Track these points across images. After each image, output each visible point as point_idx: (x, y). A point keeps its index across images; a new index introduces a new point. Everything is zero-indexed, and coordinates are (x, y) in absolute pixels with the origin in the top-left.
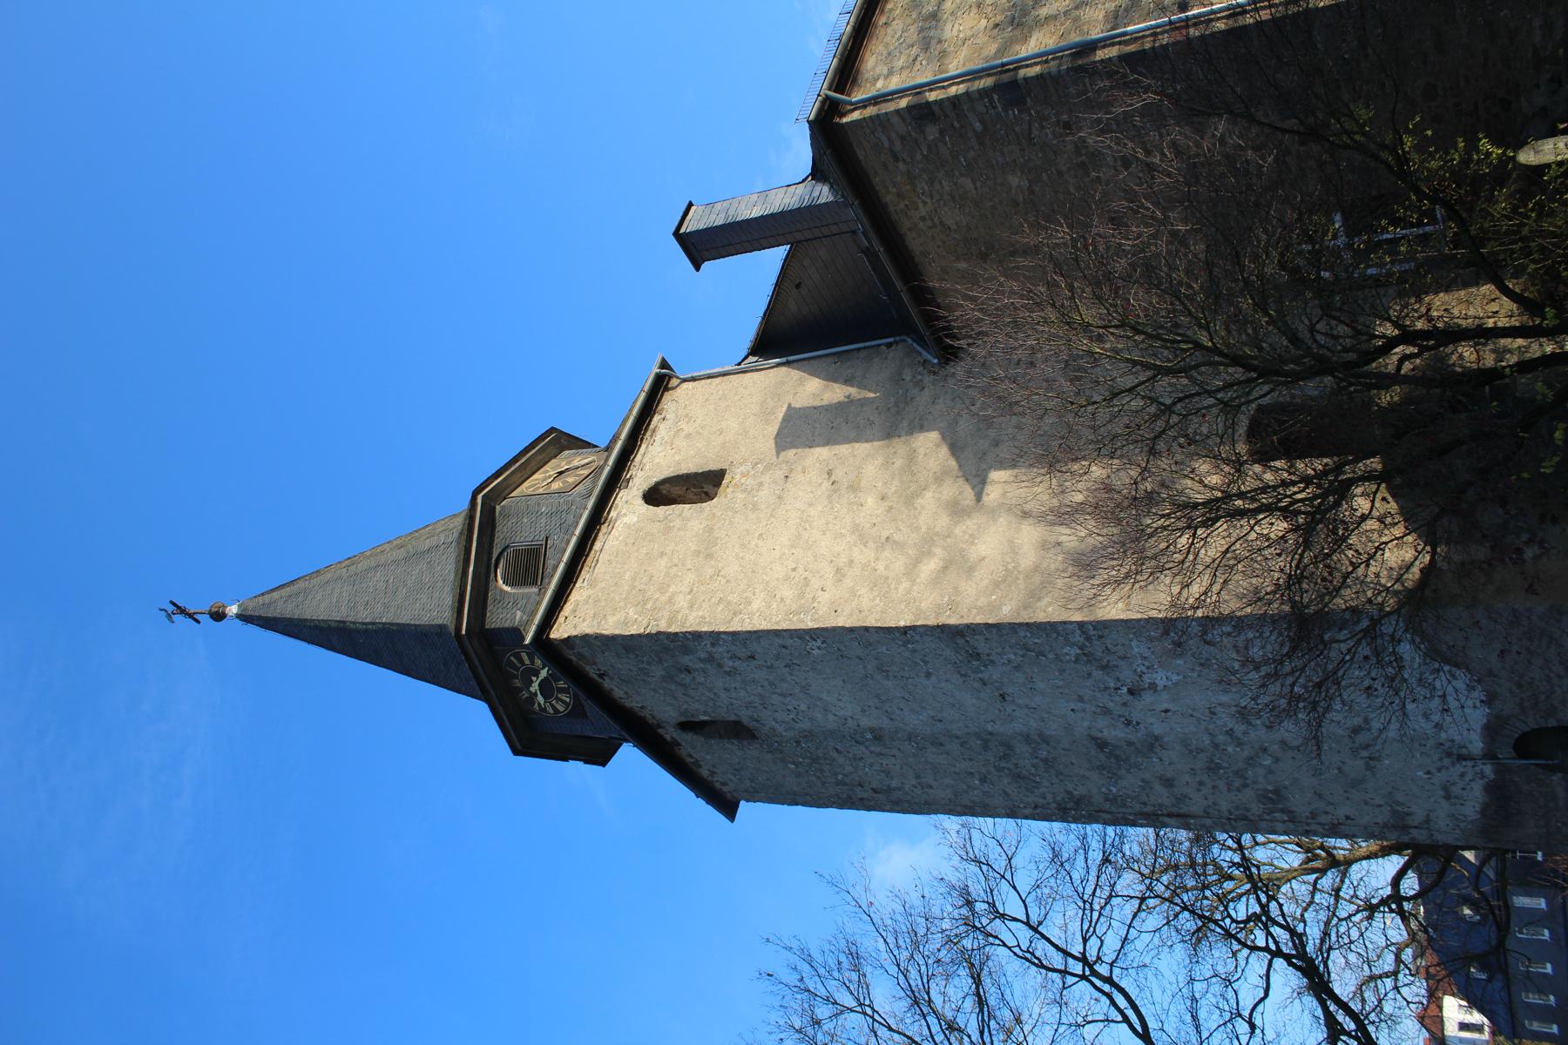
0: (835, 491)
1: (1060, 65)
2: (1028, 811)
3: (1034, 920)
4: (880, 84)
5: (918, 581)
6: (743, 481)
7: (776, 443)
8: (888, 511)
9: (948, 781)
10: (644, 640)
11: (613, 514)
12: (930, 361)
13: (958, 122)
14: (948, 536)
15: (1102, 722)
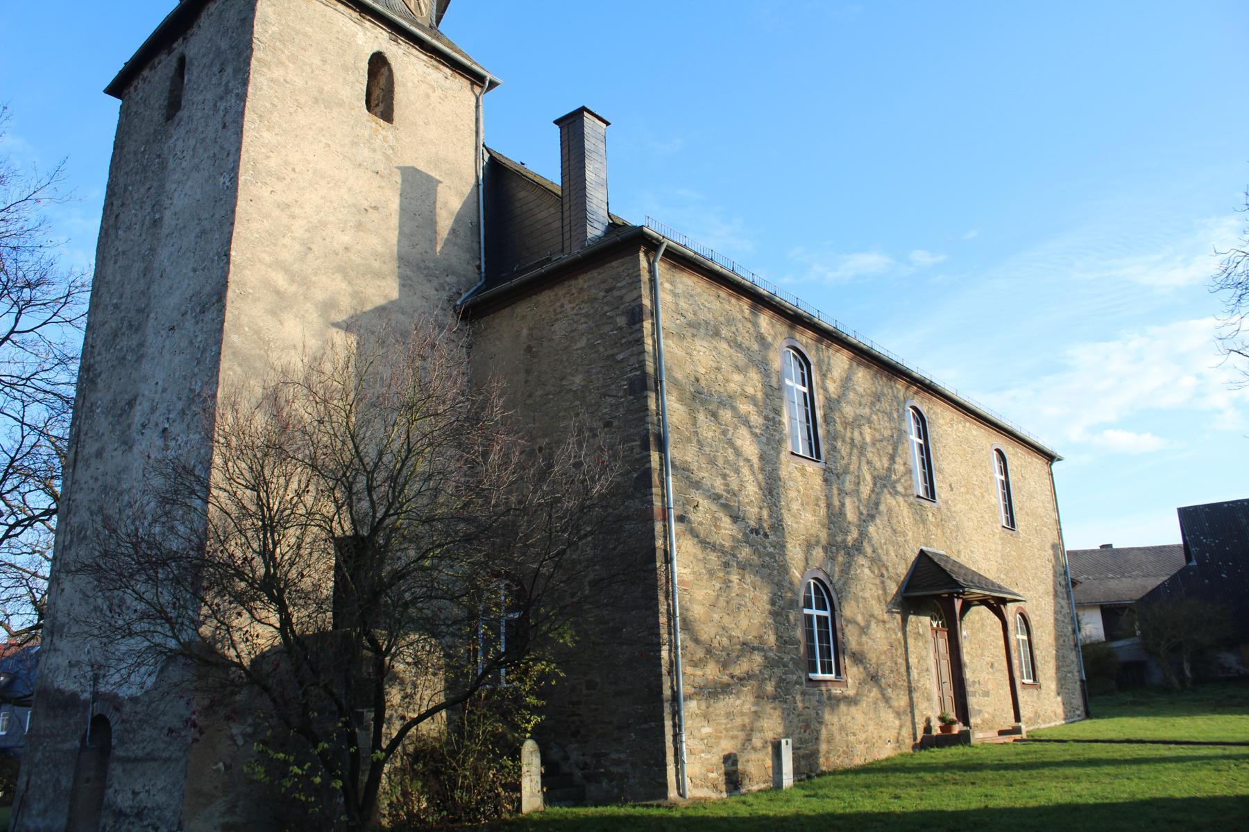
0: (359, 211)
1: (652, 424)
2: (90, 340)
3: (15, 337)
4: (667, 286)
5: (270, 270)
6: (380, 136)
7: (409, 168)
8: (334, 251)
9: (118, 278)
10: (249, 37)
11: (368, 24)
12: (459, 298)
13: (625, 343)
14: (305, 298)
15: (146, 405)
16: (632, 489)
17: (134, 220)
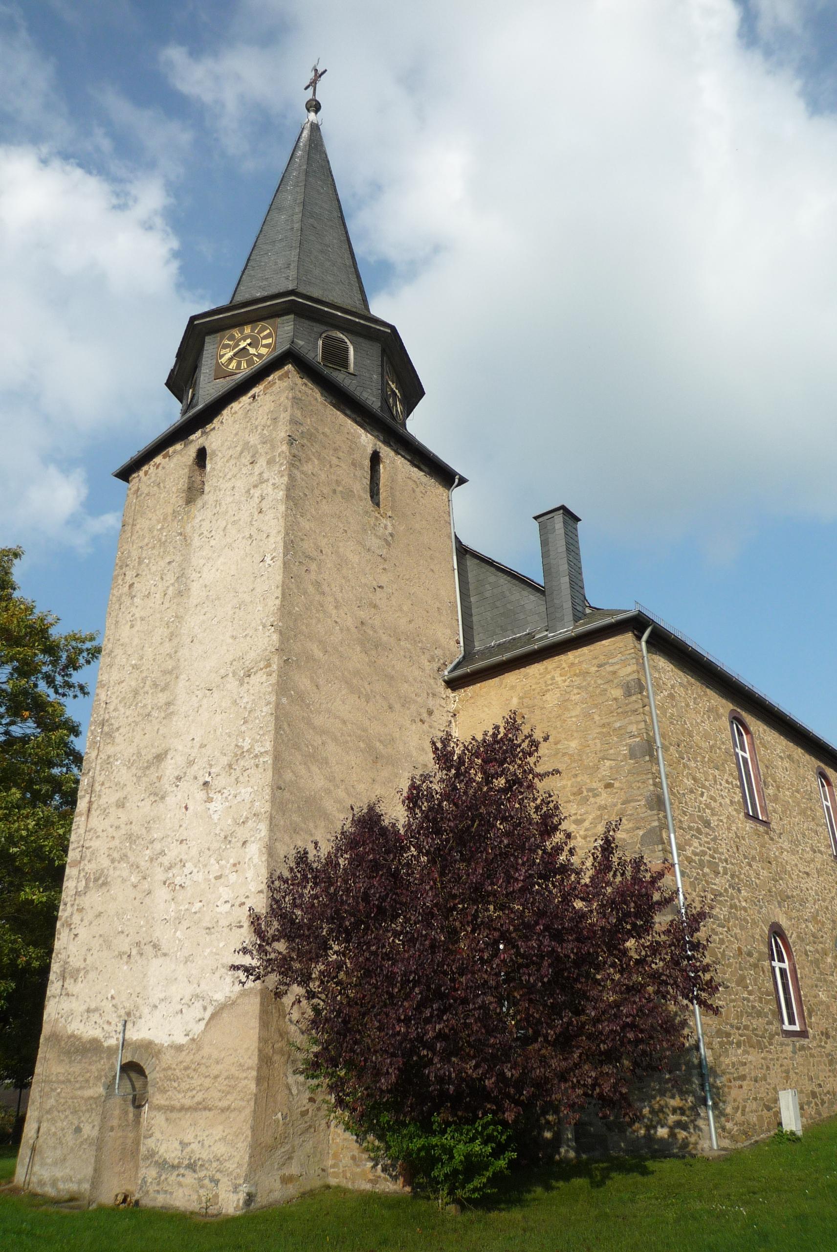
9: (136, 641)
15: (180, 760)
16: (639, 845)
17: (153, 589)
